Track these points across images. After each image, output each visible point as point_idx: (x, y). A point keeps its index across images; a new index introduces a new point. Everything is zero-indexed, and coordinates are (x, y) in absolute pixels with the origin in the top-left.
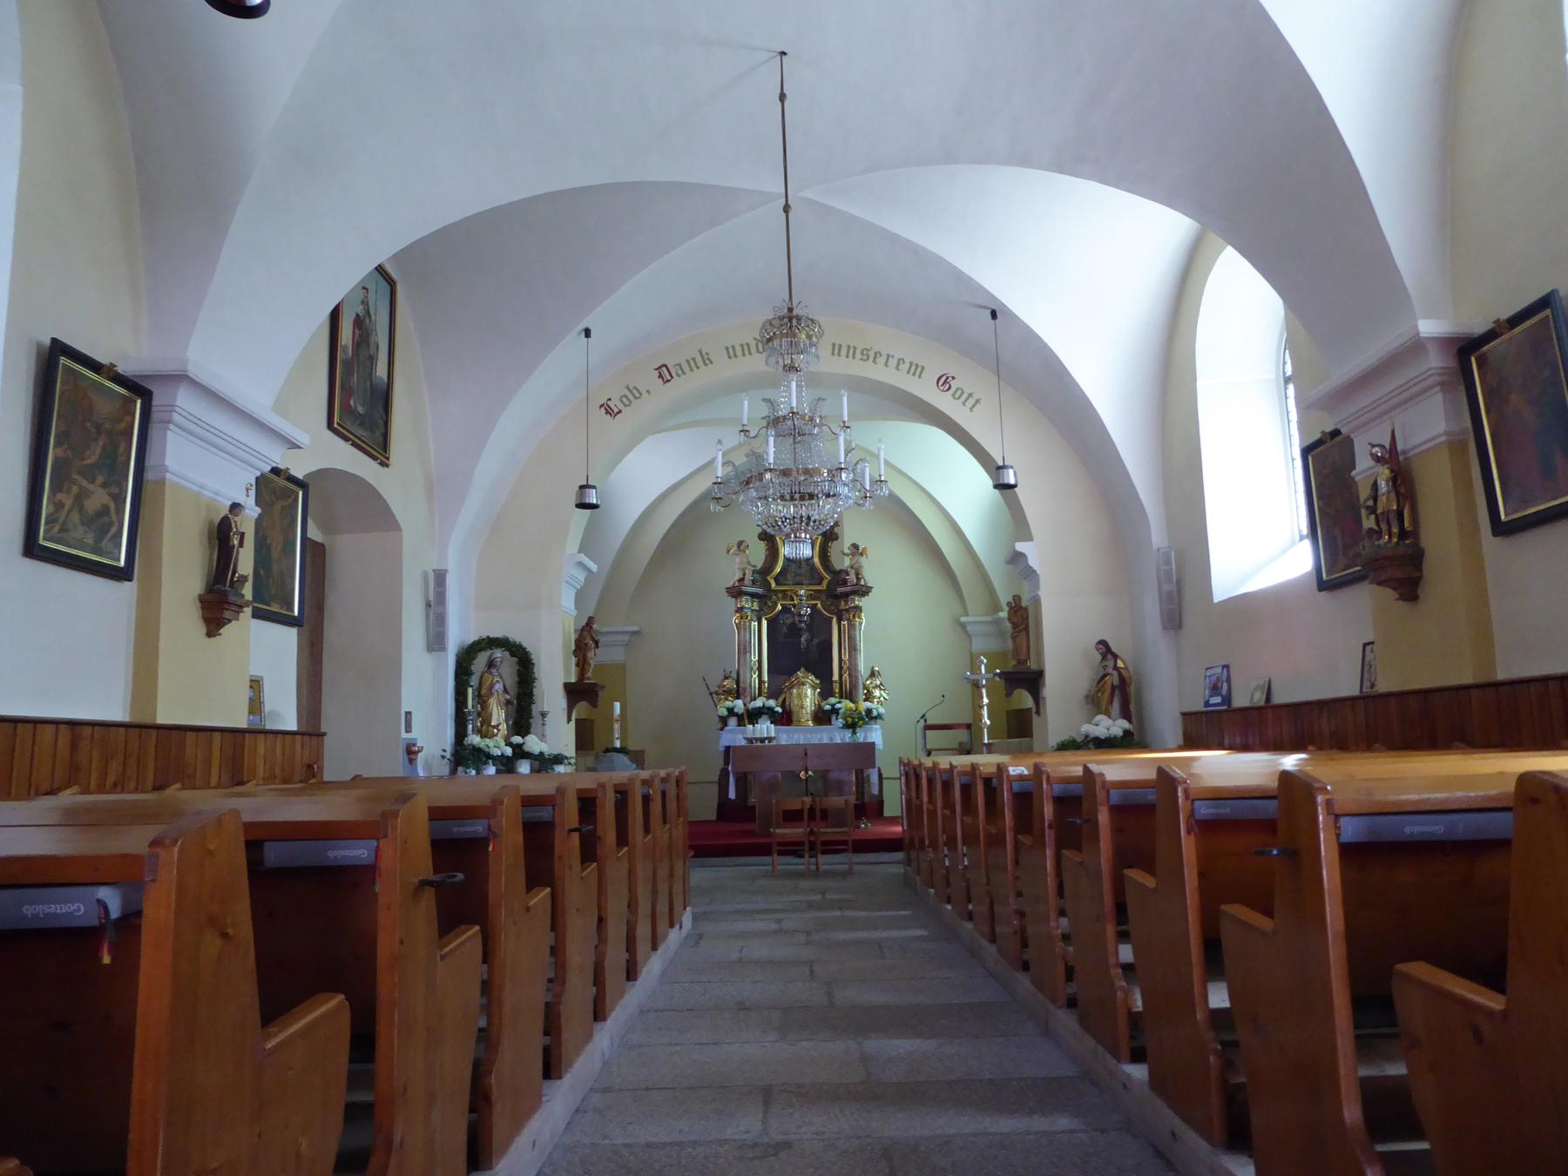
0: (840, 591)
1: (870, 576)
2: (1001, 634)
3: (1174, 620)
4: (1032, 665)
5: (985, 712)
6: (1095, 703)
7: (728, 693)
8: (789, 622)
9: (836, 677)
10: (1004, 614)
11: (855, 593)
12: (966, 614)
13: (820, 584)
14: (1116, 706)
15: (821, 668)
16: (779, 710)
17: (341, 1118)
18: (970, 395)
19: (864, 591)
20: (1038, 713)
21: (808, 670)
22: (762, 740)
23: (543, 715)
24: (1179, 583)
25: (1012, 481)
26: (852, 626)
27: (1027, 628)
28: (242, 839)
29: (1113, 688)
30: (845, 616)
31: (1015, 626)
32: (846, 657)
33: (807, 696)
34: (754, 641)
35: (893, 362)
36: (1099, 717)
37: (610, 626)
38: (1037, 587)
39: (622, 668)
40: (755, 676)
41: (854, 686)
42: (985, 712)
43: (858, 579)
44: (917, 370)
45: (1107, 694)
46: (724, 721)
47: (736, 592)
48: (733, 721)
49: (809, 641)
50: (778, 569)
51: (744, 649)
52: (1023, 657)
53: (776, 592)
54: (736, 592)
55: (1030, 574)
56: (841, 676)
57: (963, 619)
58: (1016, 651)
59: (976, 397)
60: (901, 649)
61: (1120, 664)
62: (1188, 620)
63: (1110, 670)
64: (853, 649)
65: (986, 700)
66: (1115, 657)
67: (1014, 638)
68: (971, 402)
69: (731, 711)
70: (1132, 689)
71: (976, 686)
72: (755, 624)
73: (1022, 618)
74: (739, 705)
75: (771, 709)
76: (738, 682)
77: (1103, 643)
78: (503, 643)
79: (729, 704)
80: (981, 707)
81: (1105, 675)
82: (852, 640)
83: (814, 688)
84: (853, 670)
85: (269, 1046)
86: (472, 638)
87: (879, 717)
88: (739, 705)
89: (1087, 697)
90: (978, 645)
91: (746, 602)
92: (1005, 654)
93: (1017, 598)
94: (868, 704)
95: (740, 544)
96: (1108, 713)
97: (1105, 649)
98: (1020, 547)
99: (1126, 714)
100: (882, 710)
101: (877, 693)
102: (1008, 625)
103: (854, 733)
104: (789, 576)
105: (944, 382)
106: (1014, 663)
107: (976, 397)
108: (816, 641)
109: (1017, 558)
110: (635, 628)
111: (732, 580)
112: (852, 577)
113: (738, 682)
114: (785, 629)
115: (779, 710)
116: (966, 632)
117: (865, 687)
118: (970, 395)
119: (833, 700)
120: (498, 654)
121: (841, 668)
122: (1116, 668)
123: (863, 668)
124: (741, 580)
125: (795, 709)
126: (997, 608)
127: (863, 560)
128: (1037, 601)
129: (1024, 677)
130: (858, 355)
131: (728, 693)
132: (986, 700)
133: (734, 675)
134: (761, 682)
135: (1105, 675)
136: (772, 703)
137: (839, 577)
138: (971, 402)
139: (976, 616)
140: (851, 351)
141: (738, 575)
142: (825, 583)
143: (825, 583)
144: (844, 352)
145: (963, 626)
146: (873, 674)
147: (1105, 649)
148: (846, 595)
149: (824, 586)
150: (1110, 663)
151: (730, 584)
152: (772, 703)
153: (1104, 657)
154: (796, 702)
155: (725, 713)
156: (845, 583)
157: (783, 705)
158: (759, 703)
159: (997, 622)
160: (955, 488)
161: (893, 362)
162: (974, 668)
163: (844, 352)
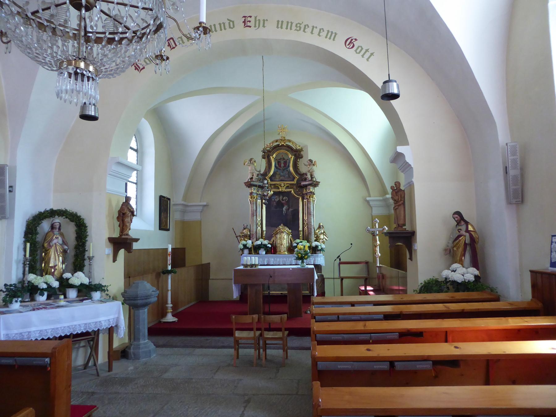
0: (304, 185)
1: (318, 177)
2: (388, 206)
3: (517, 196)
4: (408, 228)
5: (378, 249)
6: (452, 254)
8: (277, 200)
9: (301, 229)
10: (389, 196)
11: (310, 185)
12: (370, 196)
13: (293, 180)
14: (467, 258)
15: (292, 222)
16: (270, 246)
18: (367, 50)
19: (315, 184)
20: (411, 259)
21: (285, 225)
22: (252, 266)
23: (90, 259)
24: (522, 169)
25: (396, 91)
26: (309, 202)
27: (404, 204)
29: (465, 244)
30: (306, 197)
31: (396, 202)
32: (306, 218)
33: (284, 238)
35: (316, 31)
36: (455, 266)
37: (177, 199)
38: (411, 175)
39: (199, 223)
40: (259, 228)
41: (309, 233)
42: (378, 249)
43: (312, 177)
44: (332, 35)
45: (461, 250)
46: (242, 250)
47: (249, 185)
48: (246, 251)
50: (271, 173)
51: (254, 214)
52: (401, 222)
54: (249, 185)
55: (407, 168)
56: (303, 228)
57: (368, 199)
58: (397, 218)
59: (371, 51)
60: (336, 211)
61: (470, 228)
62: (531, 195)
63: (463, 232)
64: (309, 214)
65: (378, 242)
66: (467, 223)
67: (395, 209)
68: (367, 55)
69: (245, 246)
70: (478, 246)
71: (374, 235)
73: (401, 197)
74: (249, 243)
75: (265, 245)
77: (458, 213)
78: (52, 213)
79: (244, 242)
80: (376, 246)
81: (459, 236)
82: (308, 208)
83: (288, 234)
84: (309, 224)
86: (34, 211)
87: (322, 250)
88: (249, 243)
89: (446, 250)
90: (376, 211)
91: (254, 190)
92: (389, 216)
93: (398, 184)
94: (317, 243)
95: (251, 160)
96: (461, 262)
97: (459, 218)
98: (400, 149)
99: (475, 263)
100: (323, 246)
101: (322, 237)
102: (392, 201)
103: (303, 262)
104: (277, 177)
105: (350, 43)
106: (395, 226)
107: (371, 51)
109: (398, 158)
110: (205, 203)
111: (247, 179)
112: (309, 176)
115: (270, 246)
116: (370, 205)
117: (315, 234)
118: (367, 50)
119: (298, 241)
120: (57, 220)
121: (303, 224)
122: (467, 231)
123: (315, 223)
124: (252, 178)
125: (278, 245)
126: (386, 193)
127: (314, 168)
128: (411, 185)
129: (401, 241)
130: (294, 27)
132: (378, 242)
135: (459, 236)
136: (266, 242)
137: (302, 177)
138: (367, 55)
139: (374, 197)
140: (289, 25)
141: (250, 176)
142: (296, 180)
143: (296, 180)
144: (284, 26)
145: (368, 202)
146: (320, 227)
147: (459, 218)
148: (306, 186)
149: (295, 182)
150: (463, 228)
151: (246, 181)
152: (266, 242)
153: (458, 223)
154: (278, 241)
155: (242, 247)
156: (305, 180)
158: (259, 242)
159: (385, 200)
160: (361, 122)
161: (316, 31)
162: (373, 226)
163: (284, 26)
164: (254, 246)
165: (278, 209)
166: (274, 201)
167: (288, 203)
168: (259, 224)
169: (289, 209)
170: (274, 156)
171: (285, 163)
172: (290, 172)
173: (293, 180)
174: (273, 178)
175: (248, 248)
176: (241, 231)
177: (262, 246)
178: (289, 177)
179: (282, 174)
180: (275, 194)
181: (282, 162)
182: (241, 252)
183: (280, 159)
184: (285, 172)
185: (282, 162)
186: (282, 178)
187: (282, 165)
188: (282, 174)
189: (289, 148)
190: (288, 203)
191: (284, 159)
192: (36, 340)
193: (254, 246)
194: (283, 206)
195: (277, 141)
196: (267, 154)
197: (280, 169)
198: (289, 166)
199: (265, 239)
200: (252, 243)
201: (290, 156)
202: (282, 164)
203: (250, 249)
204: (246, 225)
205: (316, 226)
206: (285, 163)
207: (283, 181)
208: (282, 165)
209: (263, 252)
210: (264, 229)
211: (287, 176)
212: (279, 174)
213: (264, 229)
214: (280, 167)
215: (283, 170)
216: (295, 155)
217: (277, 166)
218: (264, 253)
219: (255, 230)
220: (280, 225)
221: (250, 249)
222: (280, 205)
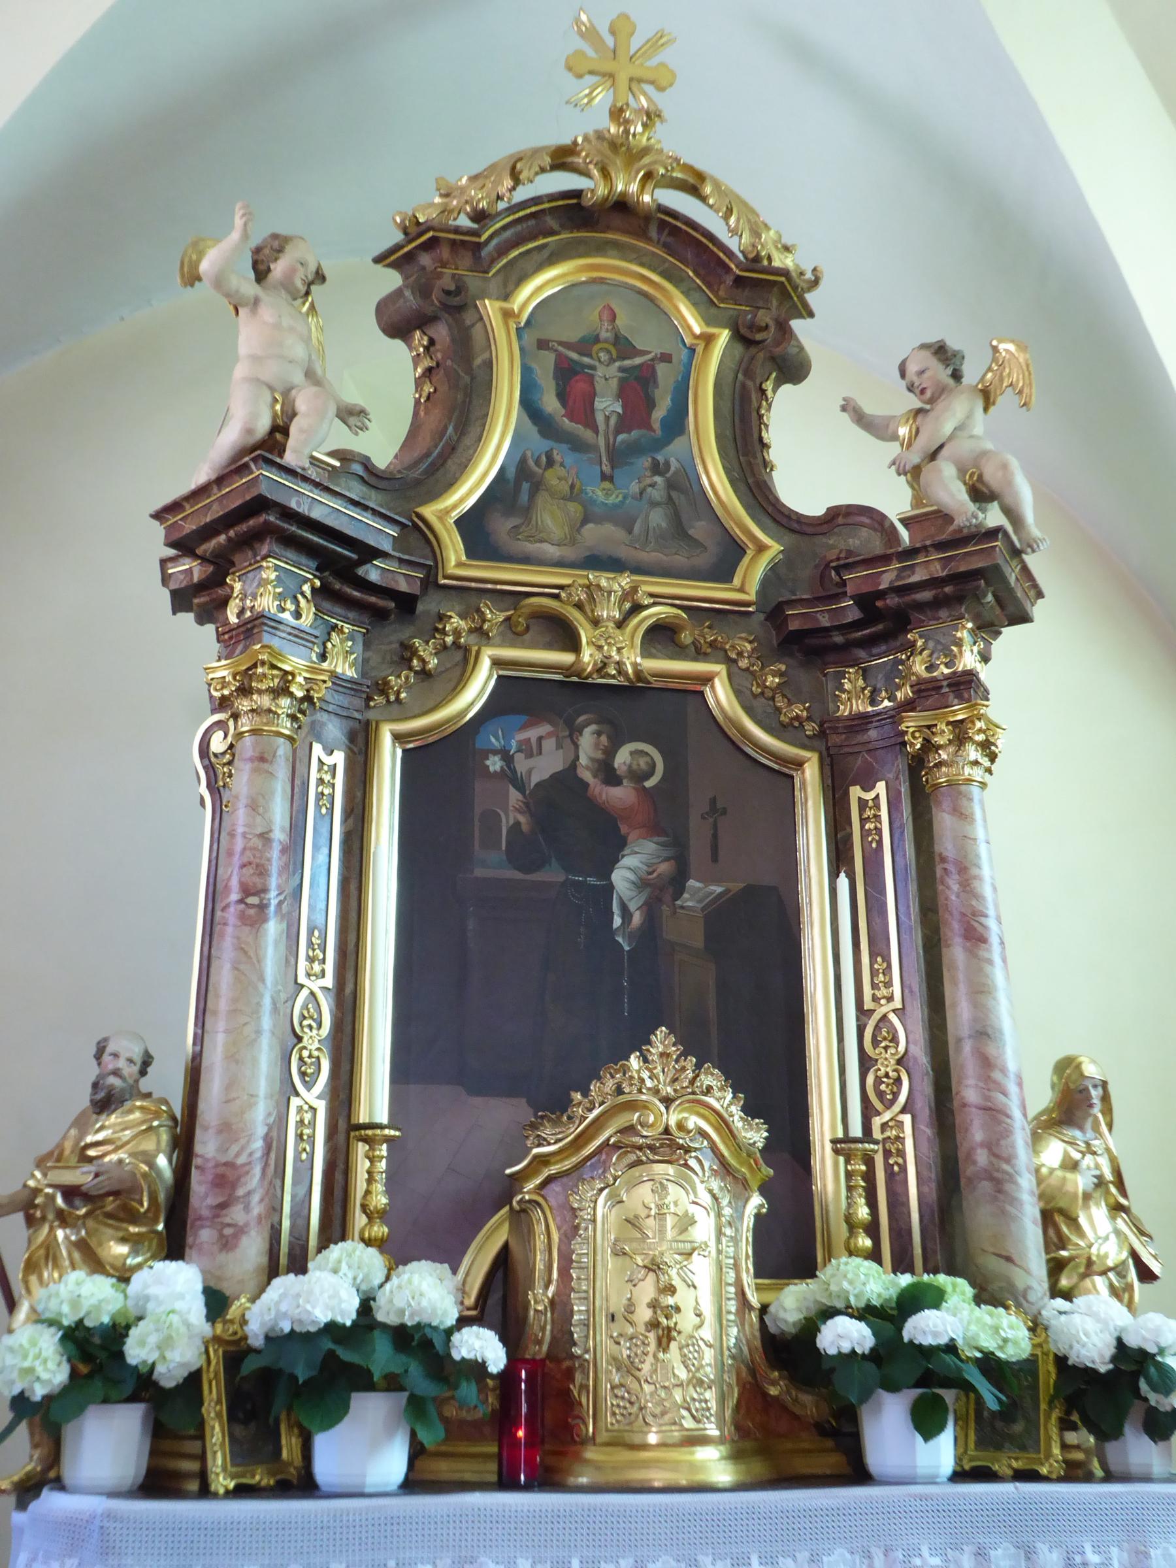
7: (102, 1203)
8: (543, 767)
13: (723, 572)
16: (483, 1346)
17: (180, 1263)
28: (199, 1287)
34: (322, 865)
40: (313, 1098)
48: (109, 1443)
49: (662, 891)
53: (469, 595)
69: (97, 1354)
72: (330, 760)
75: (419, 1343)
76: (183, 1143)
79: (86, 1294)
85: (397, 1133)
88: (168, 1309)
104: (551, 518)
108: (698, 892)
113: (183, 1143)
114: (512, 811)
115: (483, 1346)
125: (600, 1345)
131: (102, 1203)
133: (167, 1082)
134: (345, 1128)
152: (428, 1293)
155: (50, 1370)
157: (499, 1299)
158: (325, 1293)
164: (235, 1353)
165: (553, 874)
166: (511, 776)
167: (665, 812)
168: (315, 1040)
169: (677, 882)
170: (531, 293)
171: (638, 387)
172: (684, 488)
173: (723, 572)
174: (501, 526)
175: (142, 1386)
176: (53, 1131)
177: (381, 1357)
178: (679, 531)
179: (598, 493)
180: (516, 695)
181: (607, 376)
182: (20, 1454)
183: (586, 345)
184: (635, 481)
185: (607, 376)
186: (595, 535)
187: (607, 405)
188: (598, 493)
189: (688, 250)
190: (665, 812)
191: (623, 347)
192: (853, 1351)
193: (235, 1353)
194: (611, 848)
195: (562, 158)
196: (437, 279)
197: (578, 446)
198: (677, 423)
199: (398, 1253)
200: (216, 1302)
201: (691, 320)
202: (607, 403)
203: (169, 1410)
204: (128, 1049)
205: (1030, 1091)
206: (638, 387)
207: (615, 565)
208: (607, 405)
209: (365, 1449)
210: (376, 1100)
211: (658, 518)
212: (574, 494)
213: (376, 1100)
214: (584, 412)
215: (618, 457)
216: (743, 337)
217: (550, 403)
218: (392, 1464)
219: (259, 1116)
220: (639, 1042)
221: (169, 1410)
222: (573, 824)
